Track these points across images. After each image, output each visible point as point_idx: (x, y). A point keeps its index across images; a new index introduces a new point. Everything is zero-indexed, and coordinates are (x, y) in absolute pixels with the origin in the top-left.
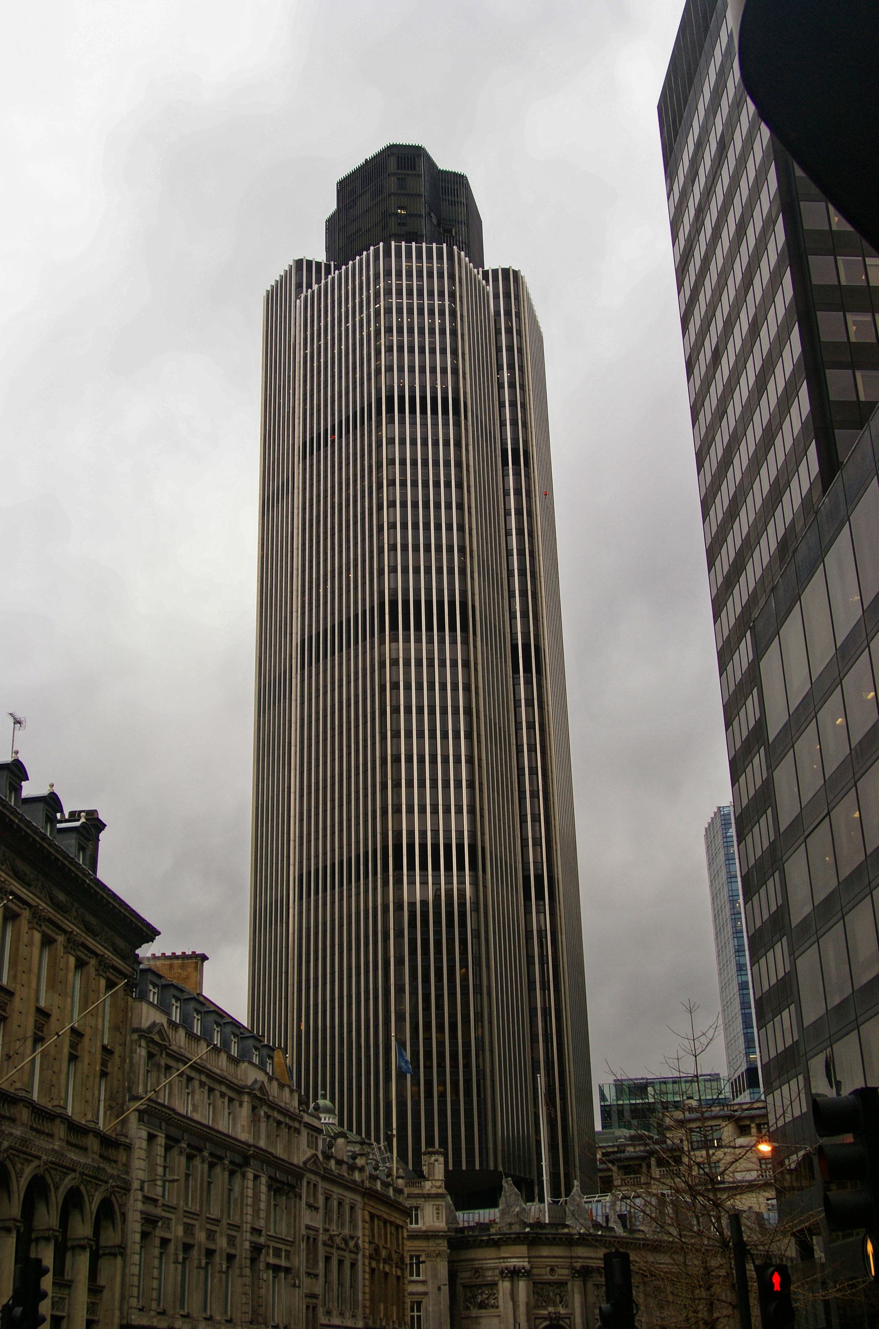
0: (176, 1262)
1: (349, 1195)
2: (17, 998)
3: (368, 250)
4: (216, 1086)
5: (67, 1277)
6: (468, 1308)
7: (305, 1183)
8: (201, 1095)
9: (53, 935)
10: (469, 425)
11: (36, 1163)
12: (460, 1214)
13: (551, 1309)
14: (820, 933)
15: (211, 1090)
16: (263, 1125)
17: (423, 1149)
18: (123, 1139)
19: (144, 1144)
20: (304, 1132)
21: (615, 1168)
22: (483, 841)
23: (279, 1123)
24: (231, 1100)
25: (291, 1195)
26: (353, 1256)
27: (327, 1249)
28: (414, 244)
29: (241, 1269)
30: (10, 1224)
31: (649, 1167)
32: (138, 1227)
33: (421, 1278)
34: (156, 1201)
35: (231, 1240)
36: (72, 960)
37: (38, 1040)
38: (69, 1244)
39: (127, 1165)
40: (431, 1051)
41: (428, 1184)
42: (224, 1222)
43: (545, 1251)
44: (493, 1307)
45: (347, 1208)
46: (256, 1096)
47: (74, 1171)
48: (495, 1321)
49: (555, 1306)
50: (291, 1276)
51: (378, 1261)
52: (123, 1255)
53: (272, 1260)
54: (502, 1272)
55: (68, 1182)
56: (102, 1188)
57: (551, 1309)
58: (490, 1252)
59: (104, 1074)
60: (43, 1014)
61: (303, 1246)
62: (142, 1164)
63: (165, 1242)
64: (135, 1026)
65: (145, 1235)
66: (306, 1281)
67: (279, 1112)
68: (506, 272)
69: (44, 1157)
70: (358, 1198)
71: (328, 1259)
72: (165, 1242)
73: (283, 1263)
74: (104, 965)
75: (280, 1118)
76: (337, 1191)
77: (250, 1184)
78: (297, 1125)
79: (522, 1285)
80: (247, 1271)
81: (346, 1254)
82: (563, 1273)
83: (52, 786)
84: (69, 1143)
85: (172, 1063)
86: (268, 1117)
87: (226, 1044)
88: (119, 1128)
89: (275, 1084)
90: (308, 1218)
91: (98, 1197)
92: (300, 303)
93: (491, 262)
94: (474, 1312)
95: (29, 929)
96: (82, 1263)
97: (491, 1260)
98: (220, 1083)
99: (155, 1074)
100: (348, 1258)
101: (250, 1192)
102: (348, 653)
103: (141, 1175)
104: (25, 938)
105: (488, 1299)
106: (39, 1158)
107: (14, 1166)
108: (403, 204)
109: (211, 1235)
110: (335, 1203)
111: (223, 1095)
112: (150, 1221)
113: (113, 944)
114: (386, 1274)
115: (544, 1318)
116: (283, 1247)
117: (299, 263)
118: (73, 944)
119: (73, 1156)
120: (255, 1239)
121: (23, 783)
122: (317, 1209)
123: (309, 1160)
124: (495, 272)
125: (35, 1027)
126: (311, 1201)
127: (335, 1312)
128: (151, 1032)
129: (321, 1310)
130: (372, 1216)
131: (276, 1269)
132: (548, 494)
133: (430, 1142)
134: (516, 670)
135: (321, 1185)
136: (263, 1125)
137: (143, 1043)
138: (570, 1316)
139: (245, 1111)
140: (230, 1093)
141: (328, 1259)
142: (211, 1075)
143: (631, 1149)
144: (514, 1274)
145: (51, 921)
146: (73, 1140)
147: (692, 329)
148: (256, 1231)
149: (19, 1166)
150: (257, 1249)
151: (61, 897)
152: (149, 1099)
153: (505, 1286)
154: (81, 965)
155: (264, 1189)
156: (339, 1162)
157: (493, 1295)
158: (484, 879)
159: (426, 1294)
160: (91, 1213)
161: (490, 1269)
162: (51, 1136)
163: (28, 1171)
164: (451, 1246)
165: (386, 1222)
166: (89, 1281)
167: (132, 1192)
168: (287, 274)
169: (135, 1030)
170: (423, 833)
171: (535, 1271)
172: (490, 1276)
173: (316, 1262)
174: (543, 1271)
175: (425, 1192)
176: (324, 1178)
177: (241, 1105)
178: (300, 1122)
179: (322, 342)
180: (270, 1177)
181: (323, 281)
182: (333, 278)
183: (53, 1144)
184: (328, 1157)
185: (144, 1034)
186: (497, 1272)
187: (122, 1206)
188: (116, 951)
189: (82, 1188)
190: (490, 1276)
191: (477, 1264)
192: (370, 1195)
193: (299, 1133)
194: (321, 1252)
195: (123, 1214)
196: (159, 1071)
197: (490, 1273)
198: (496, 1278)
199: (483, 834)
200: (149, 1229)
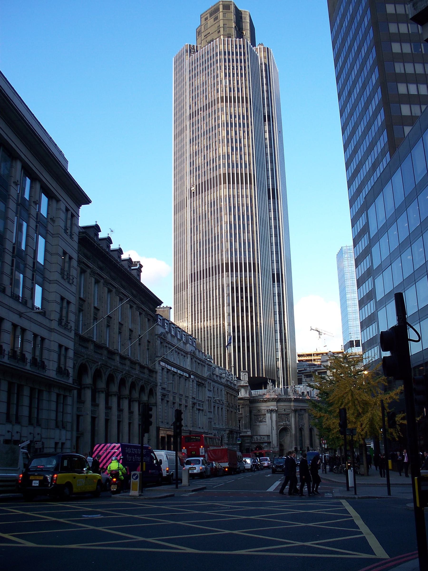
0: (171, 408)
1: (220, 386)
2: (101, 311)
4: (180, 352)
5: (121, 408)
7: (207, 383)
8: (175, 355)
9: (99, 279)
11: (132, 378)
12: (253, 391)
13: (284, 423)
14: (401, 253)
15: (179, 353)
16: (194, 364)
17: (242, 370)
18: (155, 370)
19: (161, 371)
20: (206, 366)
21: (303, 375)
22: (258, 261)
23: (199, 363)
24: (184, 356)
25: (203, 387)
26: (222, 406)
27: (214, 404)
30: (126, 396)
32: (160, 397)
33: (240, 413)
34: (165, 389)
35: (186, 401)
36: (93, 280)
37: (95, 319)
38: (121, 397)
39: (156, 378)
40: (244, 337)
41: (242, 382)
42: (184, 396)
43: (282, 404)
45: (220, 390)
47: (142, 380)
48: (265, 426)
50: (203, 412)
51: (229, 407)
52: (156, 406)
53: (198, 407)
54: (267, 411)
55: (141, 383)
56: (150, 385)
57: (284, 423)
58: (264, 404)
59: (148, 349)
60: (131, 331)
61: (207, 403)
62: (161, 378)
63: (168, 401)
64: (156, 333)
66: (208, 414)
67: (199, 360)
69: (113, 367)
70: (223, 387)
71: (214, 407)
72: (168, 401)
73: (201, 408)
74: (147, 314)
75: (199, 362)
76: (216, 385)
78: (204, 364)
79: (274, 415)
80: (191, 411)
81: (220, 405)
82: (288, 411)
83: (96, 222)
86: (196, 361)
87: (176, 334)
88: (153, 367)
89: (197, 351)
90: (208, 394)
91: (149, 388)
94: (258, 424)
96: (88, 394)
97: (264, 407)
98: (181, 351)
99: (163, 349)
100: (220, 407)
103: (160, 381)
106: (133, 376)
107: (89, 366)
109: (180, 399)
110: (216, 389)
111: (182, 355)
112: (164, 395)
114: (232, 411)
116: (201, 403)
118: (138, 308)
119: (142, 375)
121: (99, 233)
122: (211, 391)
123: (208, 375)
125: (94, 314)
126: (209, 389)
127: (217, 424)
128: (161, 335)
129: (213, 423)
130: (227, 393)
131: (199, 410)
133: (244, 368)
135: (212, 383)
136: (194, 364)
137: (159, 339)
138: (290, 425)
139: (189, 360)
140: (184, 354)
141: (214, 407)
143: (308, 369)
144: (271, 411)
145: (98, 274)
146: (121, 362)
147: (343, 76)
150: (194, 404)
151: (135, 292)
153: (268, 415)
154: (97, 282)
155: (195, 385)
156: (217, 376)
157: (265, 418)
158: (259, 275)
159: (242, 418)
162: (135, 369)
163: (130, 380)
165: (231, 395)
166: (92, 401)
169: (157, 335)
171: (279, 410)
172: (263, 412)
173: (211, 408)
174: (281, 410)
175: (242, 385)
176: (213, 381)
177: (187, 358)
180: (197, 381)
184: (213, 374)
185: (159, 336)
186: (266, 411)
187: (155, 391)
188: (150, 309)
189: (145, 385)
190: (263, 412)
192: (226, 386)
194: (213, 405)
195: (156, 393)
196: (164, 347)
197: (263, 411)
199: (258, 259)
200: (164, 398)
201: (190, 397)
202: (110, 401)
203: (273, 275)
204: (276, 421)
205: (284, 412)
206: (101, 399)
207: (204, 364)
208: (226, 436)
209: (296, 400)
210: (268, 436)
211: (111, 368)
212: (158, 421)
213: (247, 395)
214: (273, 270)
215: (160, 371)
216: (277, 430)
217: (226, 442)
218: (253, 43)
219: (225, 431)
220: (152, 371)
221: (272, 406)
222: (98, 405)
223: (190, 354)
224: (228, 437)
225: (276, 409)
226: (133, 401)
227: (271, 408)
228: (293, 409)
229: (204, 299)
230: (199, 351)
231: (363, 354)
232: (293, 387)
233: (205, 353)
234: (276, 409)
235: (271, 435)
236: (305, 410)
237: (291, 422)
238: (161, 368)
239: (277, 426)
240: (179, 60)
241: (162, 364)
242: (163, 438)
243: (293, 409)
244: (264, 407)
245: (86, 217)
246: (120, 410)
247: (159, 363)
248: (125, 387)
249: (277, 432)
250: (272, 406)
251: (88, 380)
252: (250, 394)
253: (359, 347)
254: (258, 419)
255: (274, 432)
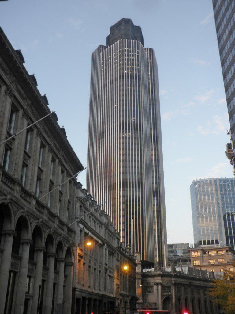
3: (118, 41)
6: (146, 292)
10: (142, 82)
12: (143, 270)
15: (95, 222)
19: (79, 232)
20: (116, 239)
24: (100, 226)
28: (129, 40)
29: (102, 275)
30: (42, 248)
31: (179, 262)
35: (100, 266)
39: (74, 238)
43: (166, 279)
44: (152, 292)
46: (106, 226)
49: (168, 292)
53: (109, 274)
54: (154, 284)
55: (58, 239)
57: (167, 293)
64: (77, 196)
65: (79, 261)
68: (150, 49)
69: (26, 209)
77: (105, 251)
79: (160, 287)
82: (169, 284)
84: (59, 227)
85: (86, 211)
86: (108, 233)
91: (67, 246)
92: (101, 54)
93: (147, 45)
94: (147, 293)
95: (48, 152)
97: (151, 281)
101: (104, 253)
102: (115, 134)
104: (46, 155)
105: (151, 290)
108: (126, 31)
111: (98, 224)
113: (71, 168)
115: (165, 295)
117: (100, 46)
120: (106, 266)
124: (147, 49)
129: (120, 289)
132: (159, 101)
134: (154, 196)
135: (120, 255)
137: (79, 202)
138: (172, 295)
139: (104, 229)
140: (99, 224)
142: (95, 217)
144: (157, 284)
148: (106, 264)
149: (45, 229)
152: (81, 219)
153: (155, 287)
156: (123, 250)
160: (65, 250)
161: (152, 282)
164: (142, 276)
167: (76, 247)
168: (98, 48)
169: (77, 197)
170: (129, 179)
172: (151, 284)
177: (102, 228)
178: (115, 236)
179: (103, 73)
181: (108, 48)
182: (104, 52)
183: (55, 225)
184: (121, 248)
185: (79, 199)
186: (153, 283)
191: (148, 282)
193: (115, 239)
198: (153, 285)
201: (104, 263)
202: (47, 262)
203: (153, 192)
204: (161, 292)
205: (166, 285)
206: (52, 263)
207: (114, 237)
208: (128, 301)
209: (176, 276)
210: (155, 304)
211: (24, 209)
212: (74, 282)
213: (140, 271)
214: (153, 188)
215: (78, 232)
216: (162, 298)
217: (129, 307)
218: (143, 46)
219: (128, 297)
220: (71, 231)
221: (159, 280)
222: (20, 259)
223: (104, 225)
224: (130, 303)
225: (161, 282)
226: (59, 261)
227: (157, 281)
228: (173, 282)
229: (111, 141)
230: (111, 225)
231: (174, 267)
232: (173, 266)
233: (115, 228)
234: (161, 282)
235: (157, 303)
236: (182, 284)
237: (172, 293)
238: (79, 230)
239: (161, 296)
240: (95, 55)
241: (82, 226)
242: (78, 300)
243: (173, 282)
244: (151, 281)
245: (24, 64)
246: (57, 272)
247: (78, 225)
248: (53, 245)
249: (162, 300)
250: (159, 280)
251: (28, 236)
252: (142, 271)
253: (212, 240)
254: (147, 290)
255: (160, 301)
